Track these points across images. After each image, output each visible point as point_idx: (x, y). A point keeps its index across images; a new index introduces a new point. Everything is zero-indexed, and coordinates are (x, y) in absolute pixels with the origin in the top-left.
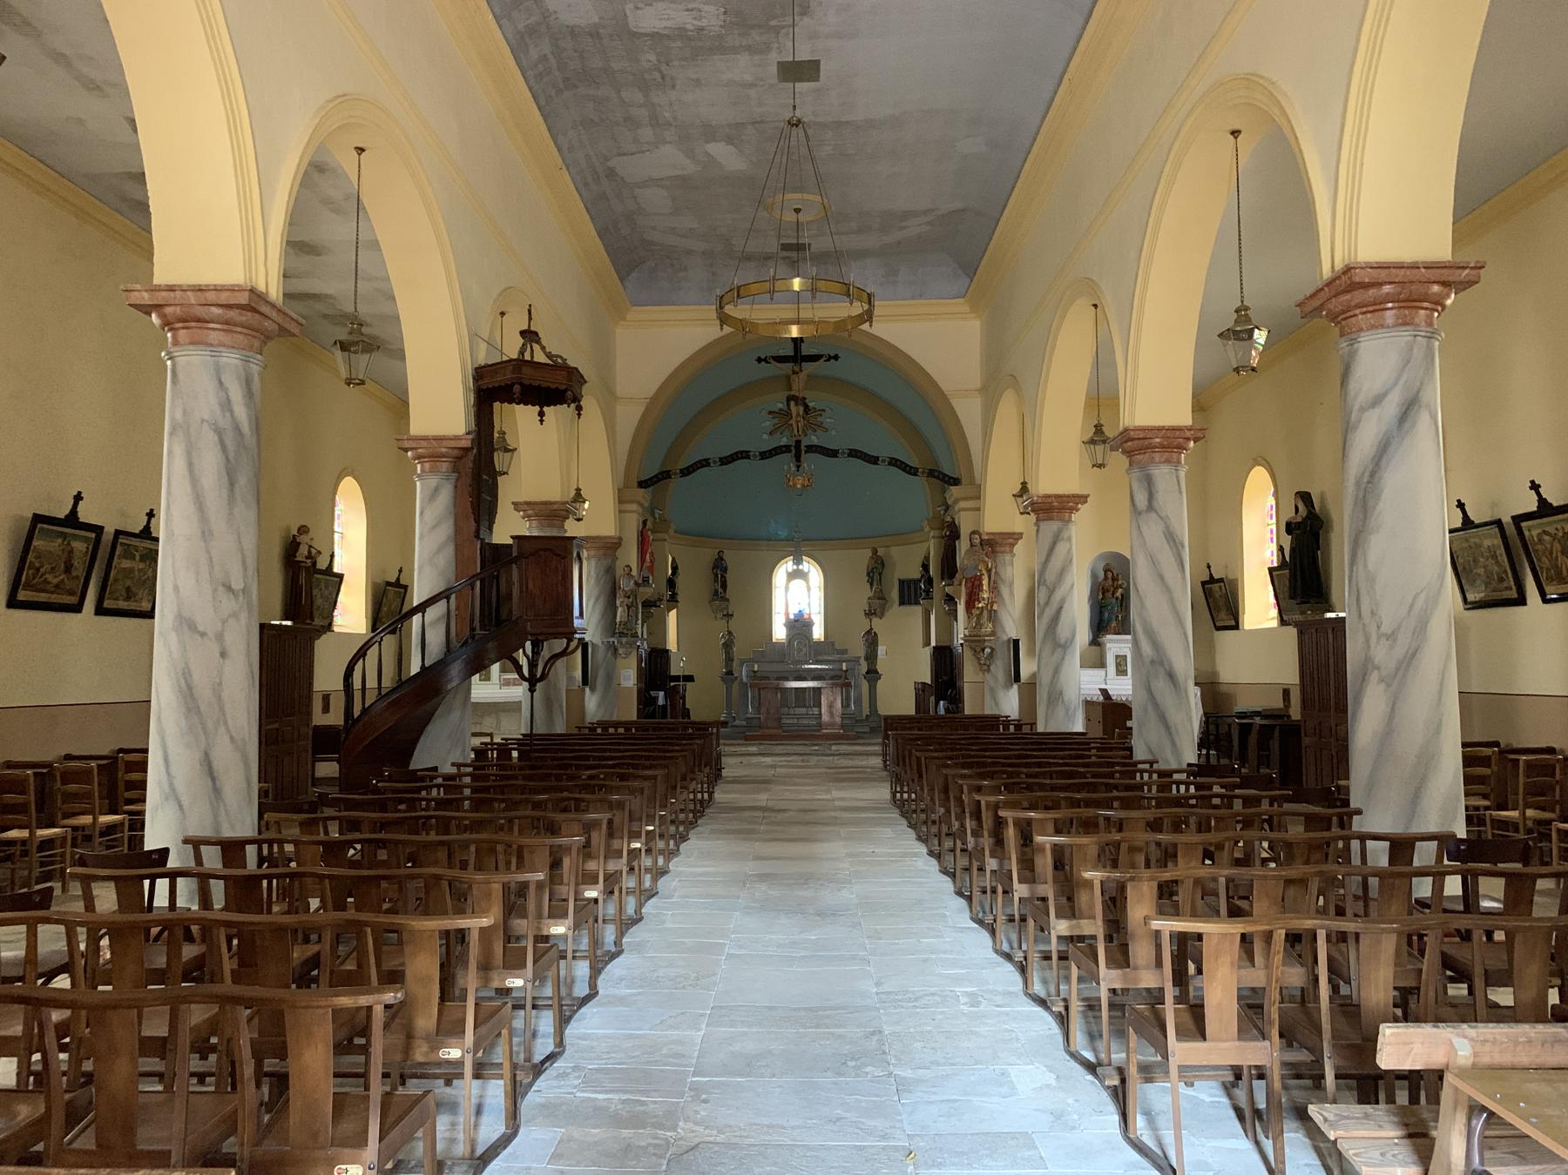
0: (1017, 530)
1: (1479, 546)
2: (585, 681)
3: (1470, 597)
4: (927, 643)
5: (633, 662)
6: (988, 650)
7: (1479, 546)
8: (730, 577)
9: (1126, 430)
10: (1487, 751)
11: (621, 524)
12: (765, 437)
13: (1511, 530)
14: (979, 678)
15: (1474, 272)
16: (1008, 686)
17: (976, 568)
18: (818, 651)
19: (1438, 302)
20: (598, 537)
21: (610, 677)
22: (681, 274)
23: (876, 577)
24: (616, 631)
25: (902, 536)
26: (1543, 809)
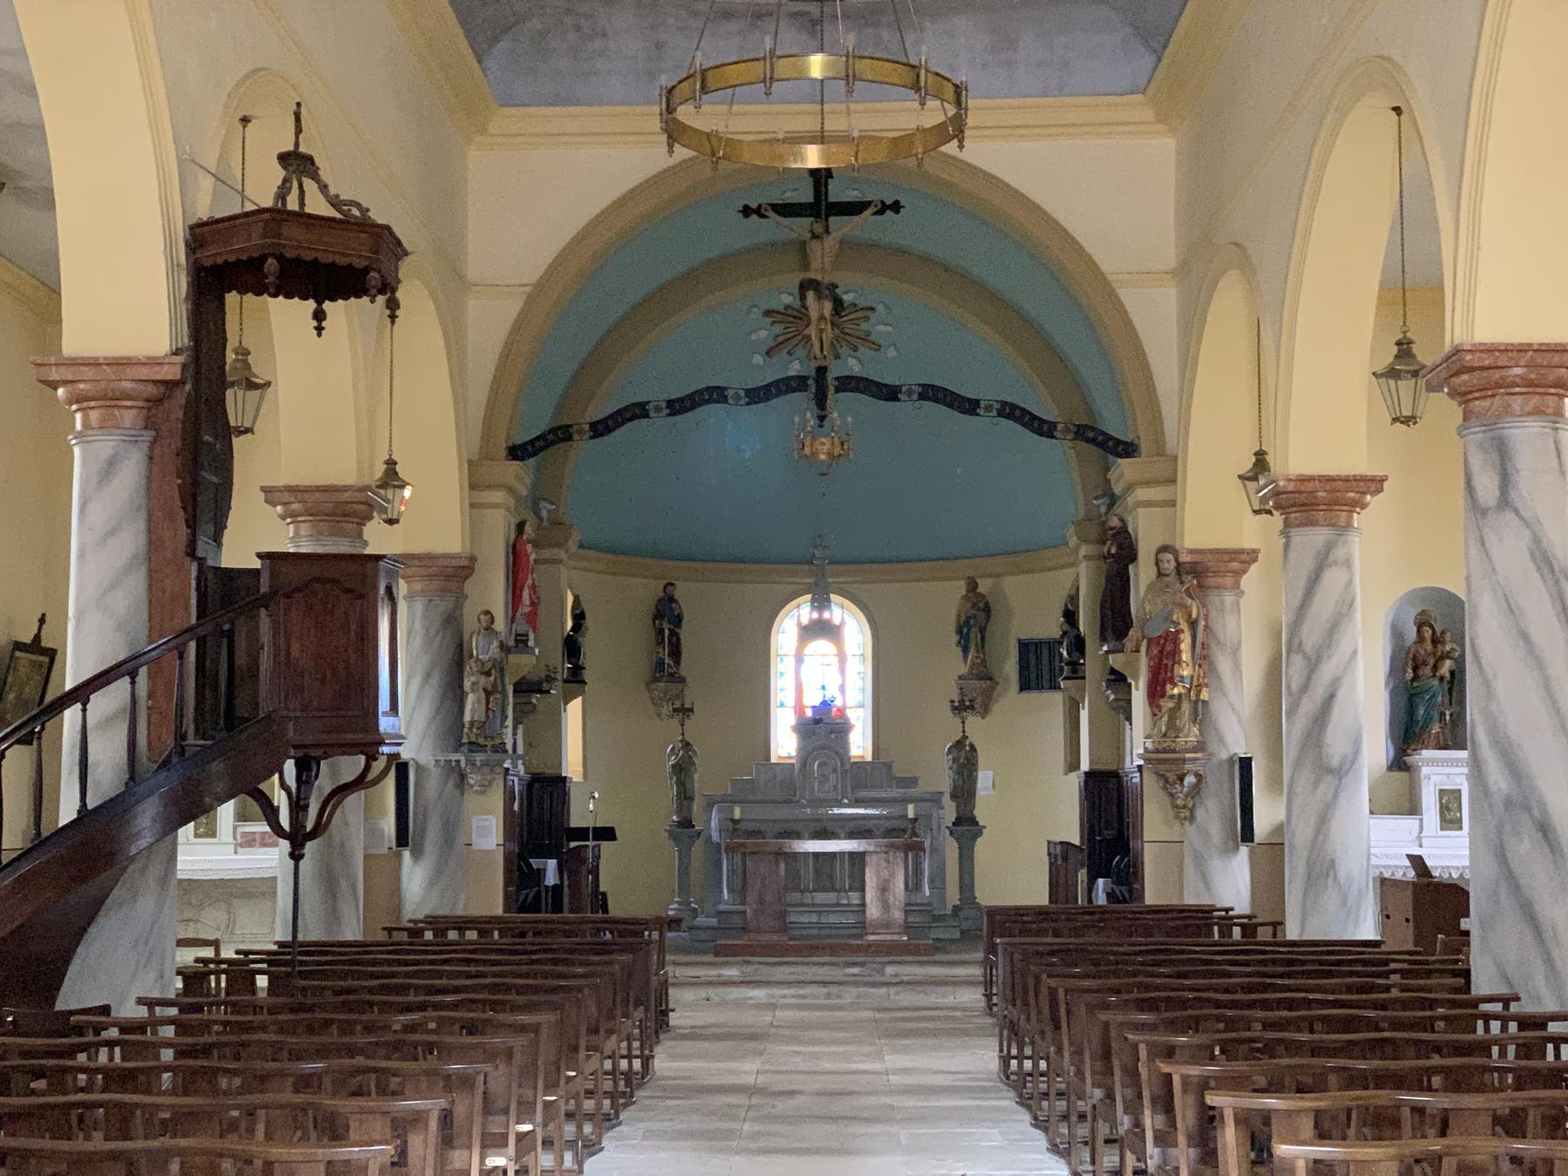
0: (1247, 544)
2: (402, 838)
5: (497, 799)
6: (1190, 780)
9: (1457, 351)
11: (474, 530)
12: (758, 359)
14: (1173, 832)
17: (1168, 618)
18: (859, 779)
21: (451, 831)
22: (598, 44)
23: (975, 635)
25: (1025, 555)
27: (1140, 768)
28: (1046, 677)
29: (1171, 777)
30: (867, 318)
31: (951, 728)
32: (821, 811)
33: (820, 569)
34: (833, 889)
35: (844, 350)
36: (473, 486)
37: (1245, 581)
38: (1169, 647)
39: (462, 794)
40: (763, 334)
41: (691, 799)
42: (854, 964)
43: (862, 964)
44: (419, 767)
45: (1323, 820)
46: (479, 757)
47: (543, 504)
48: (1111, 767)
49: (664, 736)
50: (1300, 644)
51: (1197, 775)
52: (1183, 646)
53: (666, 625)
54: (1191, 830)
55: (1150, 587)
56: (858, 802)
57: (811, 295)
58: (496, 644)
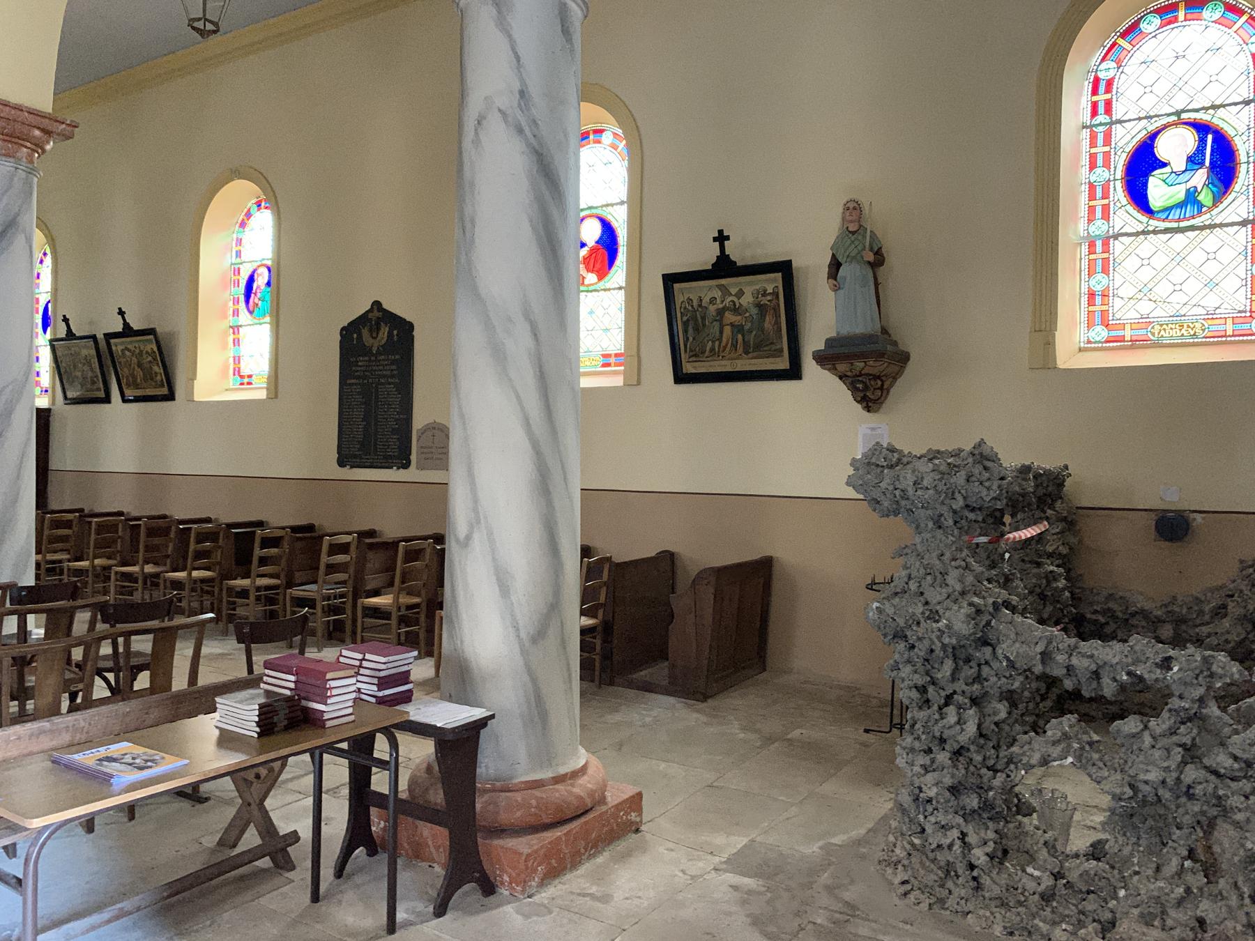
1: (78, 354)
3: (70, 395)
7: (78, 354)
10: (70, 516)
13: (102, 344)
15: (69, 129)
19: (39, 146)
26: (109, 558)
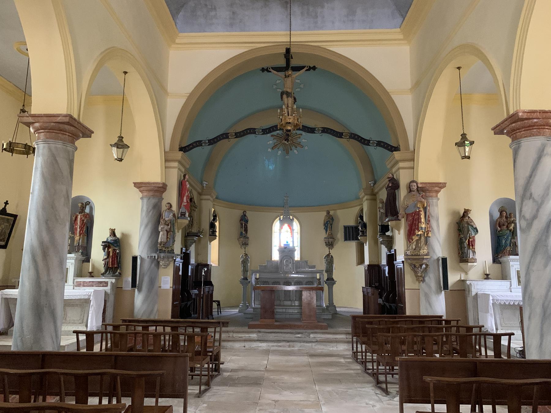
0: (441, 180)
2: (134, 285)
4: (361, 261)
5: (170, 271)
6: (424, 266)
8: (249, 225)
9: (515, 114)
11: (166, 175)
12: (269, 150)
14: (416, 286)
16: (439, 292)
17: (416, 206)
18: (298, 266)
20: (149, 183)
21: (153, 282)
22: (213, 13)
23: (329, 225)
24: (160, 249)
25: (344, 204)
27: (403, 262)
28: (355, 235)
29: (417, 265)
30: (300, 137)
31: (326, 251)
32: (287, 275)
33: (287, 210)
34: (290, 300)
35: (293, 148)
36: (166, 161)
37: (440, 195)
38: (416, 217)
39: (158, 269)
40: (271, 142)
41: (247, 271)
42: (299, 333)
43: (302, 333)
44: (142, 259)
45: (150, 267)
46: (162, 255)
47: (204, 182)
48: (376, 263)
49: (241, 252)
50: (531, 194)
51: (427, 265)
52: (421, 216)
53: (243, 223)
54: (423, 285)
55: (405, 197)
56: (297, 273)
57: (285, 96)
58: (172, 214)
